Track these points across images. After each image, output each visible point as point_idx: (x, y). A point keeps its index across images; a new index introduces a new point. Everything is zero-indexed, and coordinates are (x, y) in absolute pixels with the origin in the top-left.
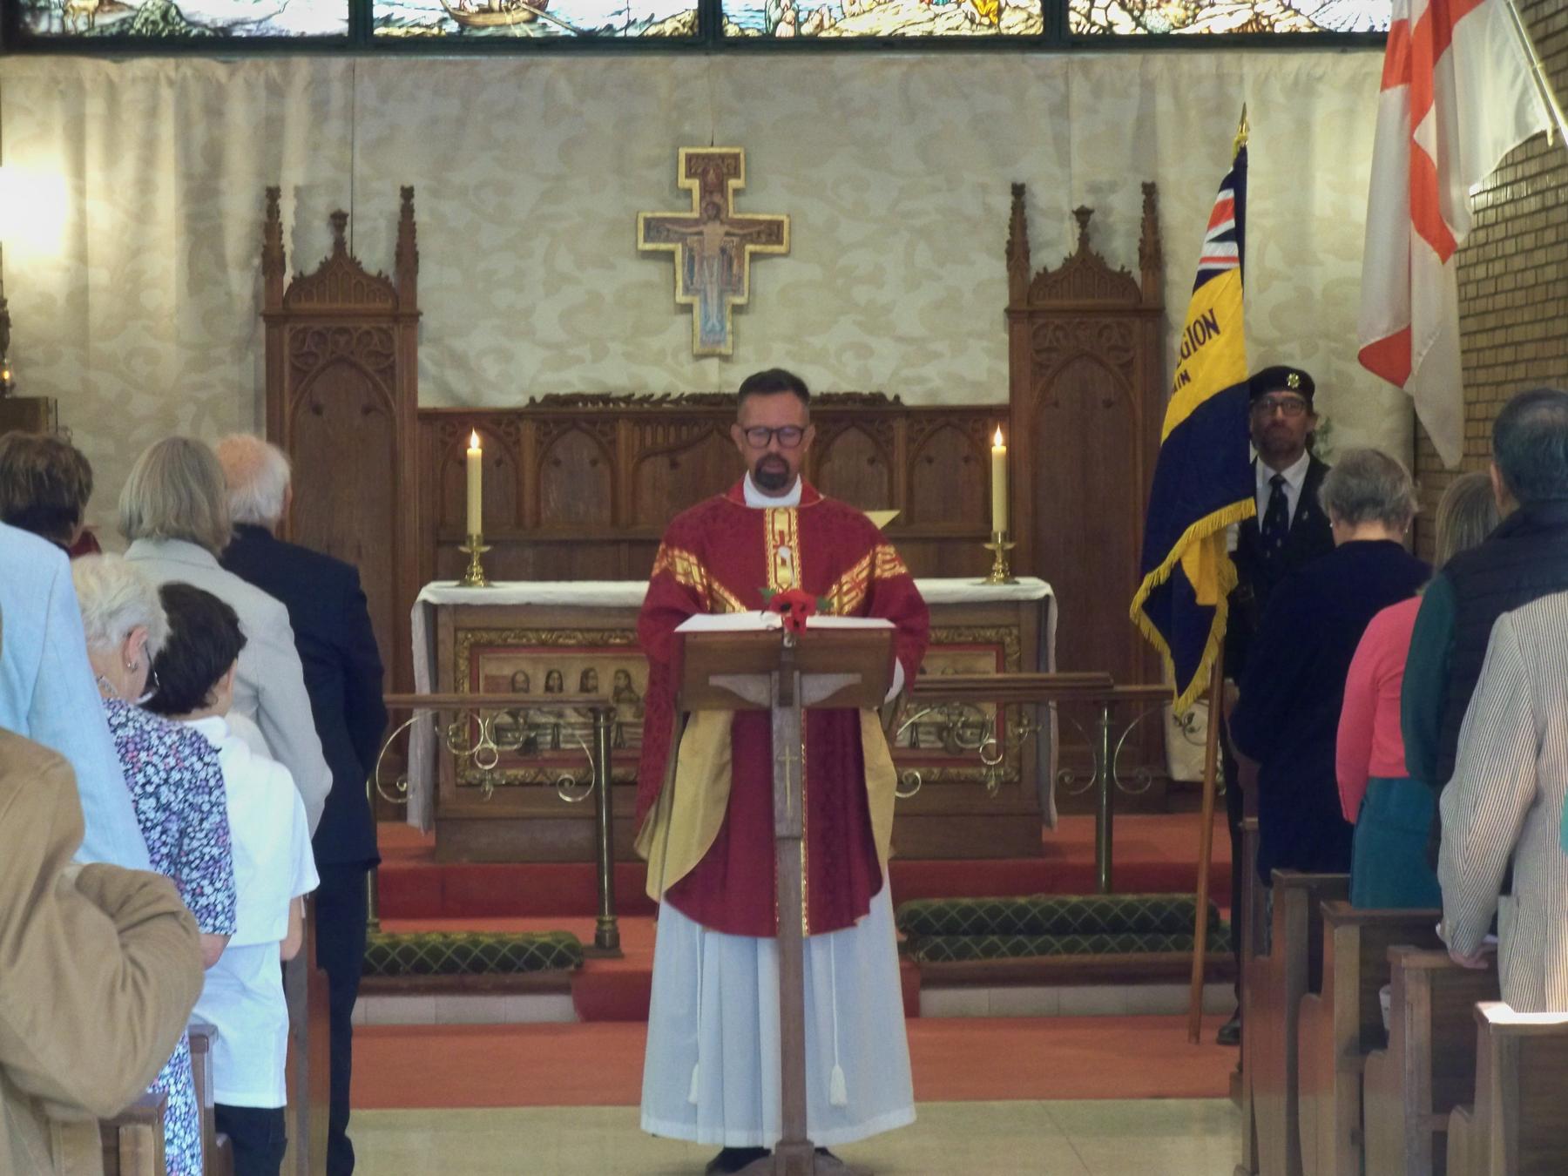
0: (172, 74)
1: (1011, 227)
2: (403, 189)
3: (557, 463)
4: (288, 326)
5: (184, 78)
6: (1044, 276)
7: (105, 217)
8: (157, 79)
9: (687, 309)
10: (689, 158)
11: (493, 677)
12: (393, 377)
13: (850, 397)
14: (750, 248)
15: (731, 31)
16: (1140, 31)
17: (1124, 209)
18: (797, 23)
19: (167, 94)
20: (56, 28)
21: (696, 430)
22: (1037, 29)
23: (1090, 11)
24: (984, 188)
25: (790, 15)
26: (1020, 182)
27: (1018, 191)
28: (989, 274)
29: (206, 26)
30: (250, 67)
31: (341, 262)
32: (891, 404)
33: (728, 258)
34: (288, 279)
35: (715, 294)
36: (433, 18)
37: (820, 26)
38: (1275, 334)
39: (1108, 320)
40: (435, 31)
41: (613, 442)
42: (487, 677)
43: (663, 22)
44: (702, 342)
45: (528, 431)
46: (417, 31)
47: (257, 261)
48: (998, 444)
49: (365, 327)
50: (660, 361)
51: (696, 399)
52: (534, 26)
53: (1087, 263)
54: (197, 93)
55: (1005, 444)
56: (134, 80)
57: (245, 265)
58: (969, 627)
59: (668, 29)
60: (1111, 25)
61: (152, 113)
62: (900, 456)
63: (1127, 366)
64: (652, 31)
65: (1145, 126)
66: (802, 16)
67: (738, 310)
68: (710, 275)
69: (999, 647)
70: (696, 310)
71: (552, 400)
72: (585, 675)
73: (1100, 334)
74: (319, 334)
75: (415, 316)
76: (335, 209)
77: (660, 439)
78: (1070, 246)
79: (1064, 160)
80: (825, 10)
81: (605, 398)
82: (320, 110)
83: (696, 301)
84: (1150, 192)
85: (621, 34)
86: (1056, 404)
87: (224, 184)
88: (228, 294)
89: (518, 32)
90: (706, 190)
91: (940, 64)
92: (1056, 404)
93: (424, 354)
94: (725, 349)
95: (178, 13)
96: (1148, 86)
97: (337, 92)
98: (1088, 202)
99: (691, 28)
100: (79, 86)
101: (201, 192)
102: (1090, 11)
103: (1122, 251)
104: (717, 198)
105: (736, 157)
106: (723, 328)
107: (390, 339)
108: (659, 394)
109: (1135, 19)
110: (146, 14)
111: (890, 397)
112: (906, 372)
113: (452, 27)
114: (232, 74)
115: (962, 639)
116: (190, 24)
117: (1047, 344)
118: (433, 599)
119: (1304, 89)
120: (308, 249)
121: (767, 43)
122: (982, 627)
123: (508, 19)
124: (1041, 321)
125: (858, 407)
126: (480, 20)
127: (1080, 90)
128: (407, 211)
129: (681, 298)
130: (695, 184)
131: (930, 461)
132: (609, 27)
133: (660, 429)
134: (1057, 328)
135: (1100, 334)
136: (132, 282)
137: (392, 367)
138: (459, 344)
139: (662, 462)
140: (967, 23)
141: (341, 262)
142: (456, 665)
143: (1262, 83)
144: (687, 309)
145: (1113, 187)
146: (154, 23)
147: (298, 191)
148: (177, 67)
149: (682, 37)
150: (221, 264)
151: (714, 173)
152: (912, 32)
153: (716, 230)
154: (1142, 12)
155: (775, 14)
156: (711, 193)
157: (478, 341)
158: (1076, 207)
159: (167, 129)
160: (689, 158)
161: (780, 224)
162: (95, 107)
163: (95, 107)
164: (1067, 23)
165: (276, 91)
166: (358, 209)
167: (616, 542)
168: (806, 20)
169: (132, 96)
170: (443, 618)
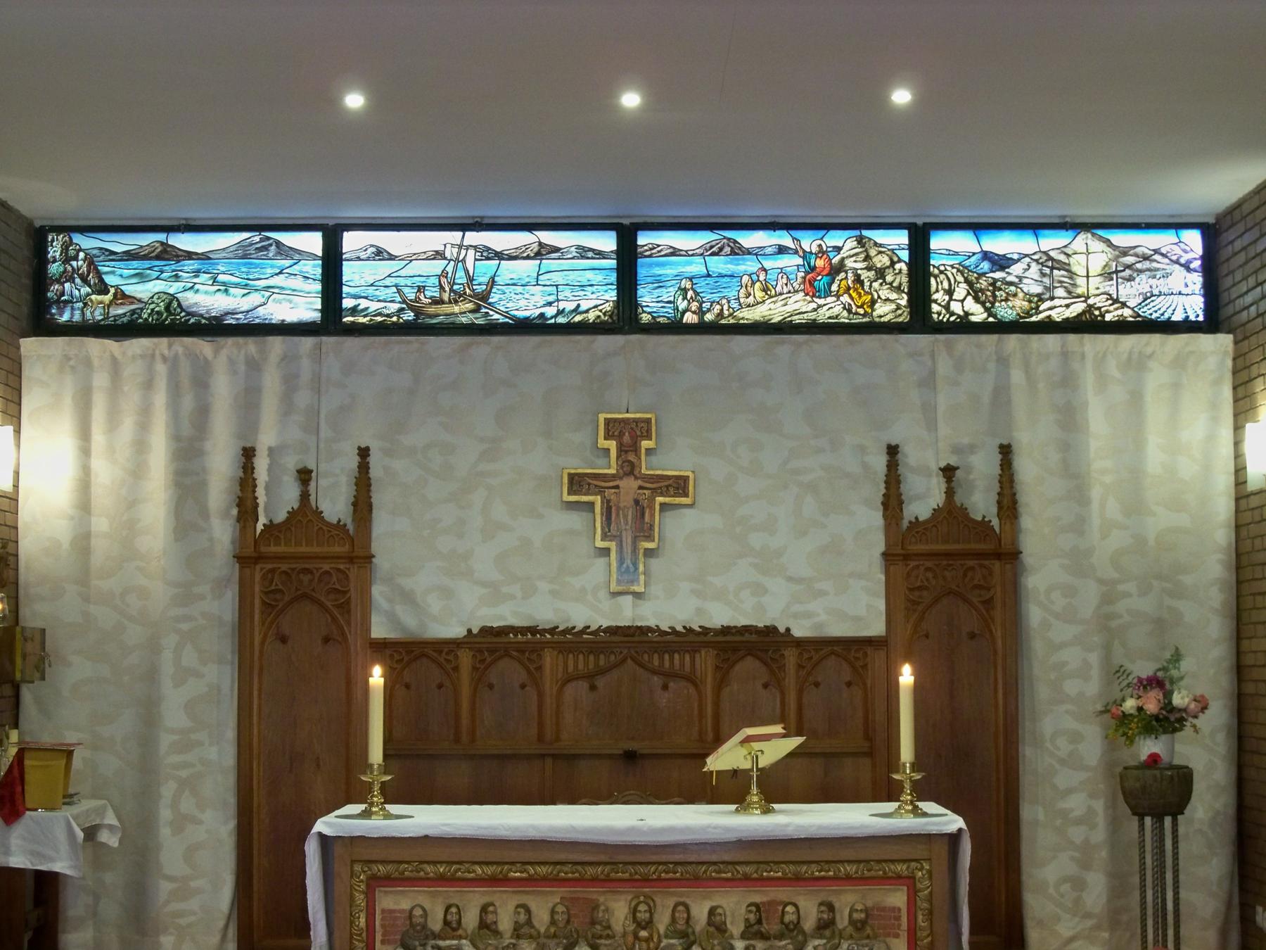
0: (166, 352)
1: (886, 482)
2: (359, 448)
3: (491, 687)
4: (258, 567)
5: (176, 357)
6: (916, 523)
7: (104, 472)
8: (153, 356)
9: (605, 552)
10: (608, 422)
11: (392, 911)
12: (349, 612)
13: (747, 629)
14: (660, 499)
15: (645, 318)
16: (991, 319)
17: (983, 467)
18: (701, 312)
19: (161, 369)
20: (77, 317)
21: (612, 658)
22: (905, 318)
23: (948, 303)
24: (862, 449)
25: (694, 306)
26: (893, 444)
27: (893, 451)
28: (865, 526)
29: (201, 316)
30: (229, 344)
31: (306, 512)
32: (782, 635)
33: (640, 509)
34: (260, 527)
35: (629, 541)
36: (394, 307)
37: (721, 314)
38: (1116, 575)
39: (971, 563)
40: (395, 319)
41: (540, 668)
42: (383, 911)
43: (587, 311)
44: (619, 582)
45: (465, 659)
46: (379, 319)
47: (235, 511)
48: (907, 676)
49: (326, 567)
50: (579, 593)
51: (613, 631)
52: (478, 315)
53: (952, 513)
54: (185, 368)
55: (384, 676)
56: (134, 357)
57: (225, 514)
58: (879, 862)
59: (591, 316)
60: (967, 314)
61: (148, 385)
62: (791, 681)
63: (988, 603)
64: (578, 318)
65: (1001, 395)
66: (706, 306)
67: (649, 553)
68: (625, 522)
69: (909, 882)
70: (613, 555)
71: (486, 631)
72: (484, 909)
73: (965, 575)
74: (285, 572)
75: (369, 558)
76: (300, 466)
77: (581, 666)
78: (936, 498)
79: (932, 425)
80: (724, 301)
81: (533, 630)
82: (290, 383)
83: (613, 545)
84: (1006, 451)
85: (552, 321)
86: (927, 636)
87: (208, 446)
88: (211, 540)
89: (464, 320)
90: (621, 450)
91: (822, 343)
92: (927, 636)
93: (378, 591)
94: (639, 588)
95: (180, 305)
96: (1003, 361)
97: (306, 366)
98: (953, 461)
99: (611, 316)
100: (88, 363)
101: (188, 453)
102: (948, 303)
103: (982, 503)
104: (631, 457)
105: (648, 421)
106: (636, 569)
107: (347, 577)
108: (580, 626)
109: (987, 310)
110: (152, 306)
111: (782, 630)
112: (797, 608)
113: (409, 316)
114: (216, 352)
115: (873, 873)
116: (188, 314)
117: (919, 584)
118: (327, 831)
119: (1137, 364)
120: (278, 500)
121: (676, 327)
122: (893, 861)
123: (456, 309)
124: (913, 564)
125: (754, 637)
126: (432, 310)
127: (944, 366)
128: (364, 467)
129: (600, 544)
130: (612, 445)
131: (817, 685)
132: (542, 315)
133: (581, 657)
134: (928, 569)
135: (965, 575)
136: (129, 529)
137: (348, 602)
138: (407, 583)
139: (583, 685)
140: (845, 313)
141: (306, 512)
142: (352, 898)
143: (1100, 361)
144: (605, 552)
145: (972, 448)
146: (159, 313)
147: (271, 450)
148: (170, 346)
149: (603, 323)
150: (205, 514)
151: (629, 435)
152: (797, 319)
153: (628, 495)
154: (993, 304)
155: (682, 305)
156: (626, 452)
157: (422, 581)
158: (943, 464)
159: (160, 399)
160: (608, 422)
161: (686, 479)
162: (101, 380)
163: (101, 380)
164: (931, 312)
165: (254, 366)
166: (323, 467)
167: (543, 756)
168: (709, 310)
169: (133, 371)
170: (338, 850)
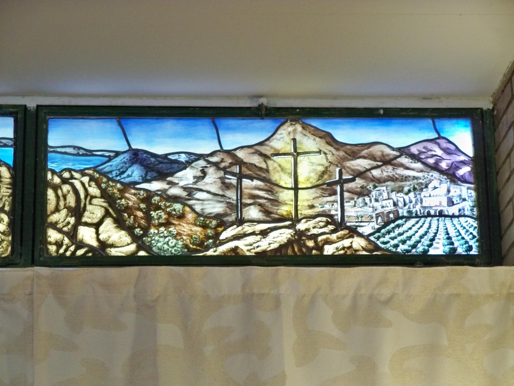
109: (135, 239)
119: (366, 315)
127: (50, 317)
143: (306, 308)
154: (146, 230)
164: (45, 242)
